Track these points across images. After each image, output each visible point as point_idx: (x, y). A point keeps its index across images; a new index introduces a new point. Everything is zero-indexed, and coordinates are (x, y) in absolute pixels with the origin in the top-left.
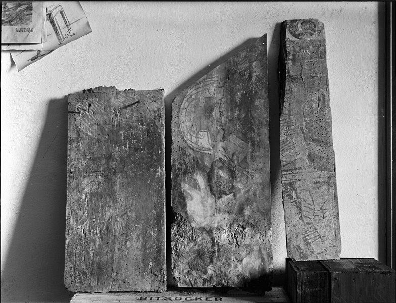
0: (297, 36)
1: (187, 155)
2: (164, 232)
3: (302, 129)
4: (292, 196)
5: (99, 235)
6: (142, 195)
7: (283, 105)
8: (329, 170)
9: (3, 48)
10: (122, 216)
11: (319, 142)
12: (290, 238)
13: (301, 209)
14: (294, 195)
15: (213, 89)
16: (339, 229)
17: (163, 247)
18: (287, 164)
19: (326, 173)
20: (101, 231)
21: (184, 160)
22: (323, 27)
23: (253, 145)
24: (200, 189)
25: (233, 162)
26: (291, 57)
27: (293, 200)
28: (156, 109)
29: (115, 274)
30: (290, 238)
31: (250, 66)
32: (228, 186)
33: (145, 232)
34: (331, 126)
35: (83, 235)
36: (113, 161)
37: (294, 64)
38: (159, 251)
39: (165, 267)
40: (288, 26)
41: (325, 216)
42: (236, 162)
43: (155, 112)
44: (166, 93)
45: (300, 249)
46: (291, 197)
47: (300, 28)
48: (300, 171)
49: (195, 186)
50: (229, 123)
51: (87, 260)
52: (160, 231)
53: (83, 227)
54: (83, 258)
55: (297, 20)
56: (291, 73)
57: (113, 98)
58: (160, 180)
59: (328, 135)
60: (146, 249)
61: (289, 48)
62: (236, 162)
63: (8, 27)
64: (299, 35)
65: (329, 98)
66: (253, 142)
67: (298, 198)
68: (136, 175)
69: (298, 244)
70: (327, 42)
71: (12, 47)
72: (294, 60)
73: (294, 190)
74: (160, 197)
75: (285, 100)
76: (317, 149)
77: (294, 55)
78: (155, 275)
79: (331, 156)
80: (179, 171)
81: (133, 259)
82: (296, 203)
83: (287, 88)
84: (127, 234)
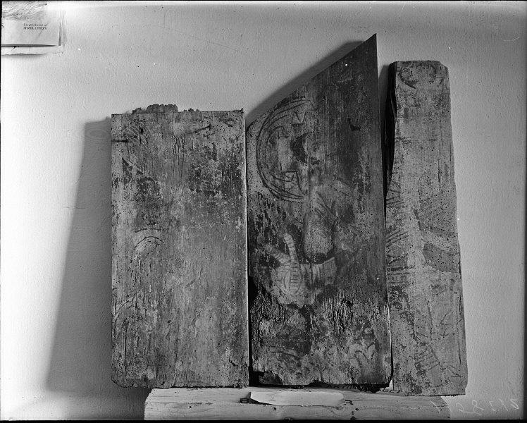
0: (411, 84)
1: (269, 205)
2: (246, 307)
3: (416, 213)
4: (401, 304)
5: (157, 311)
6: (216, 257)
7: (390, 179)
8: (452, 270)
9: (4, 51)
10: (188, 286)
11: (440, 232)
12: (398, 365)
13: (413, 324)
14: (403, 303)
15: (306, 115)
16: (464, 351)
17: (244, 328)
18: (394, 261)
19: (448, 275)
20: (159, 306)
21: (265, 212)
22: (446, 69)
23: (361, 191)
24: (288, 253)
25: (334, 214)
26: (402, 112)
27: (402, 311)
28: (234, 138)
29: (180, 363)
30: (398, 365)
31: (354, 80)
32: (327, 246)
33: (221, 311)
34: (454, 211)
35: (135, 311)
36: (175, 208)
37: (406, 122)
38: (239, 334)
39: (247, 353)
40: (398, 69)
41: (446, 333)
42: (337, 214)
43: (232, 141)
44: (246, 112)
45: (411, 379)
46: (400, 307)
47: (415, 74)
48: (412, 270)
49: (282, 248)
50: (326, 159)
51: (141, 345)
52: (241, 305)
53: (135, 300)
54: (136, 342)
55: (410, 62)
56: (402, 135)
57: (174, 122)
58: (240, 235)
59: (451, 221)
60: (221, 330)
61: (401, 100)
62: (337, 214)
63: (13, 21)
64: (414, 82)
65: (453, 170)
66: (361, 185)
67: (409, 307)
68: (207, 228)
69: (408, 372)
70: (452, 97)
71: (18, 50)
72: (406, 116)
73: (405, 296)
74: (241, 259)
75: (394, 171)
76: (438, 241)
77: (406, 110)
78: (234, 365)
79: (454, 253)
80: (259, 228)
81: (204, 344)
82: (407, 315)
83: (396, 154)
84: (195, 312)
